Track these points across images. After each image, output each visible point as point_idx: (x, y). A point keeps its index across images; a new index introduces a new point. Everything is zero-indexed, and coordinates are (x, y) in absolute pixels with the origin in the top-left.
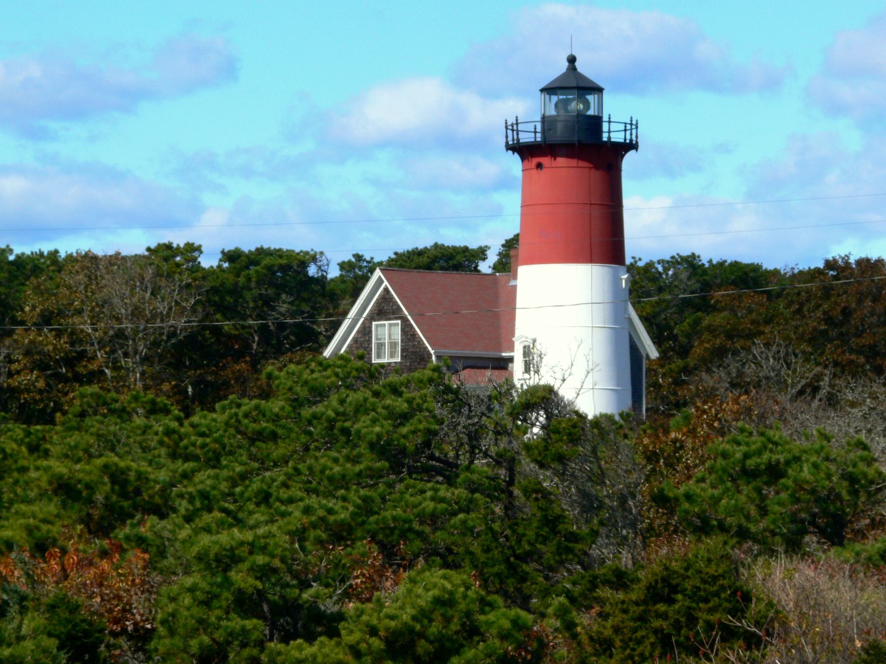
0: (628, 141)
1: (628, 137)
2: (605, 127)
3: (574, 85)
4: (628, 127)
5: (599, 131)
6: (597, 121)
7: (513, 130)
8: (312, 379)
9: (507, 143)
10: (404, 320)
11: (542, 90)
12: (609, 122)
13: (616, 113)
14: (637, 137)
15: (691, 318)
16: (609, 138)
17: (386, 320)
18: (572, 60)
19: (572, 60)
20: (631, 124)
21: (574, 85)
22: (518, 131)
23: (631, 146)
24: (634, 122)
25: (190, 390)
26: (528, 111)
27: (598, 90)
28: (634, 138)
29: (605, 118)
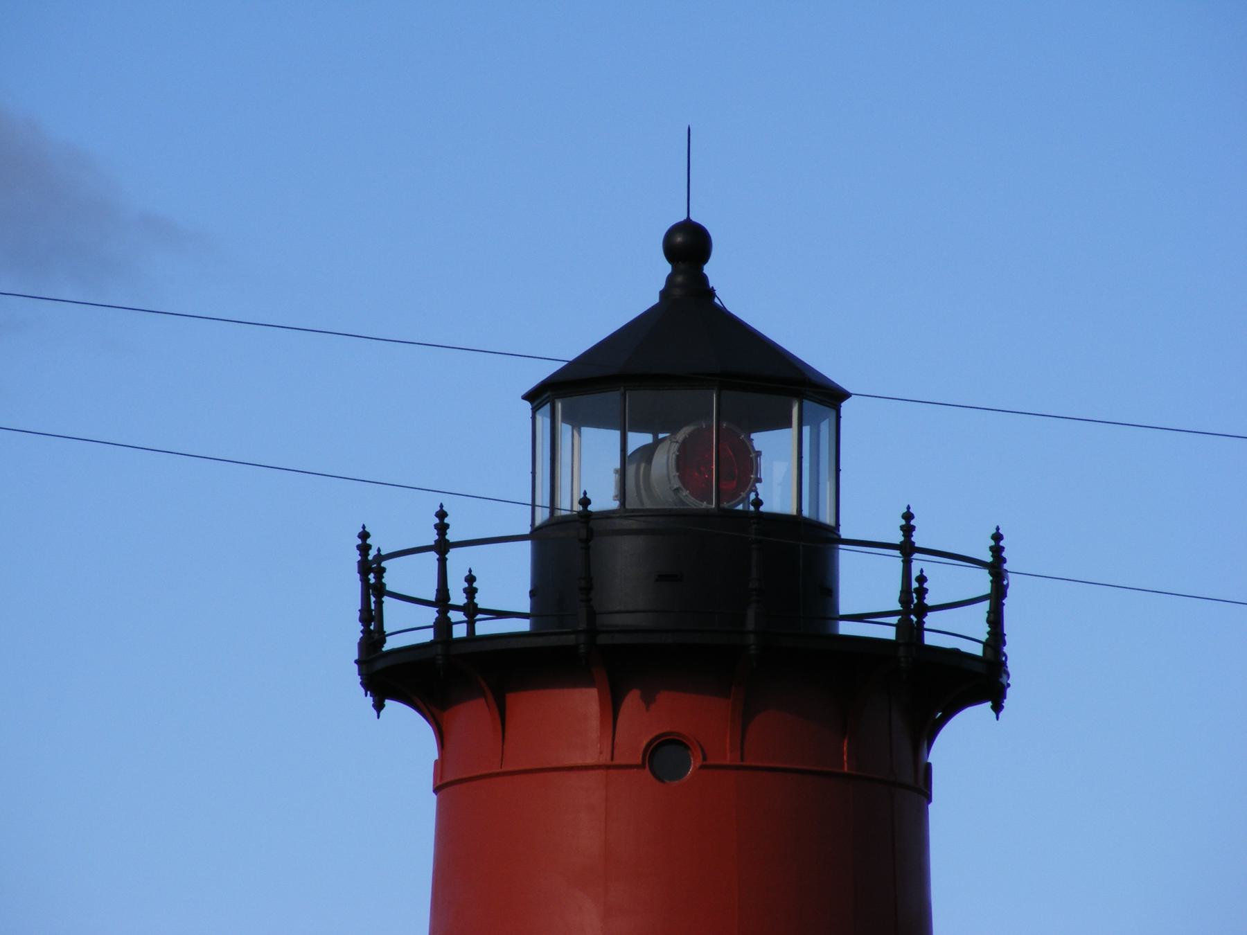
3: (691, 363)
6: (808, 547)
11: (536, 397)
13: (893, 493)
18: (688, 246)
19: (688, 246)
21: (691, 363)
23: (983, 678)
26: (483, 488)
27: (832, 396)
29: (864, 513)
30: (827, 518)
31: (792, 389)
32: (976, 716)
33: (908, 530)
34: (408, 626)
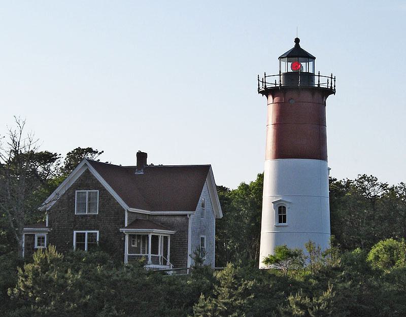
0: (329, 88)
1: (330, 85)
2: (316, 78)
3: (297, 54)
4: (330, 79)
5: (313, 81)
6: (310, 76)
7: (263, 82)
8: (50, 226)
9: (259, 88)
10: (102, 190)
11: (280, 58)
12: (319, 76)
13: (322, 70)
14: (335, 86)
15: (359, 212)
16: (319, 85)
17: (87, 190)
18: (297, 41)
19: (297, 41)
20: (332, 78)
21: (297, 54)
22: (265, 83)
23: (331, 91)
24: (333, 77)
25: (271, 286)
26: (275, 71)
27: (314, 58)
28: (333, 86)
29: (316, 73)
30: (311, 71)
31: (310, 58)
32: (331, 97)
33: (319, 74)
34: (311, 63)
